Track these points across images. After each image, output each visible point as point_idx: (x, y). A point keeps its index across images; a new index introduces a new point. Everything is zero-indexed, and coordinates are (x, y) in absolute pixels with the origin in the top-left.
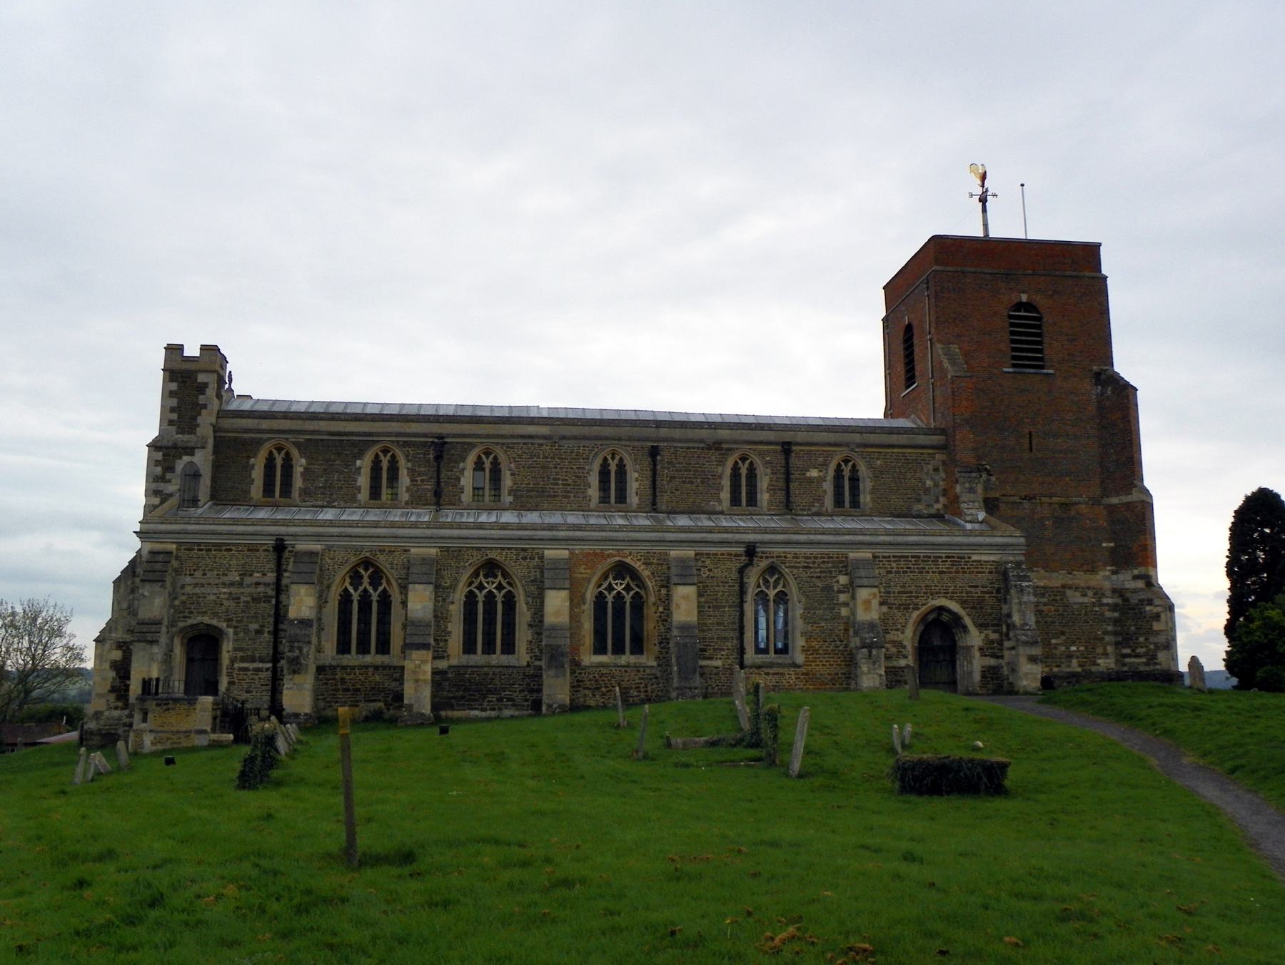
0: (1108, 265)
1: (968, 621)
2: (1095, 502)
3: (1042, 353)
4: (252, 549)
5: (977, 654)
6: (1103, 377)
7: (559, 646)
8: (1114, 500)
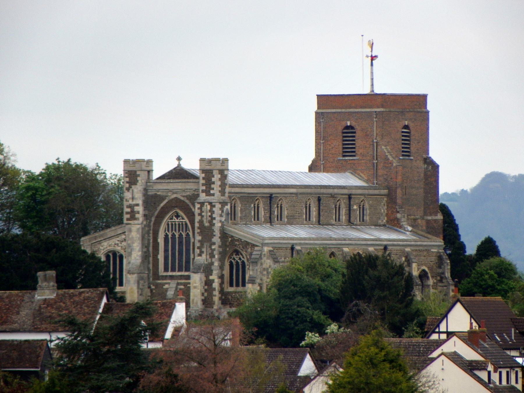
0: (430, 106)
1: (429, 275)
2: (422, 218)
3: (410, 149)
4: (286, 249)
5: (431, 288)
6: (428, 161)
7: (321, 281)
8: (429, 218)
